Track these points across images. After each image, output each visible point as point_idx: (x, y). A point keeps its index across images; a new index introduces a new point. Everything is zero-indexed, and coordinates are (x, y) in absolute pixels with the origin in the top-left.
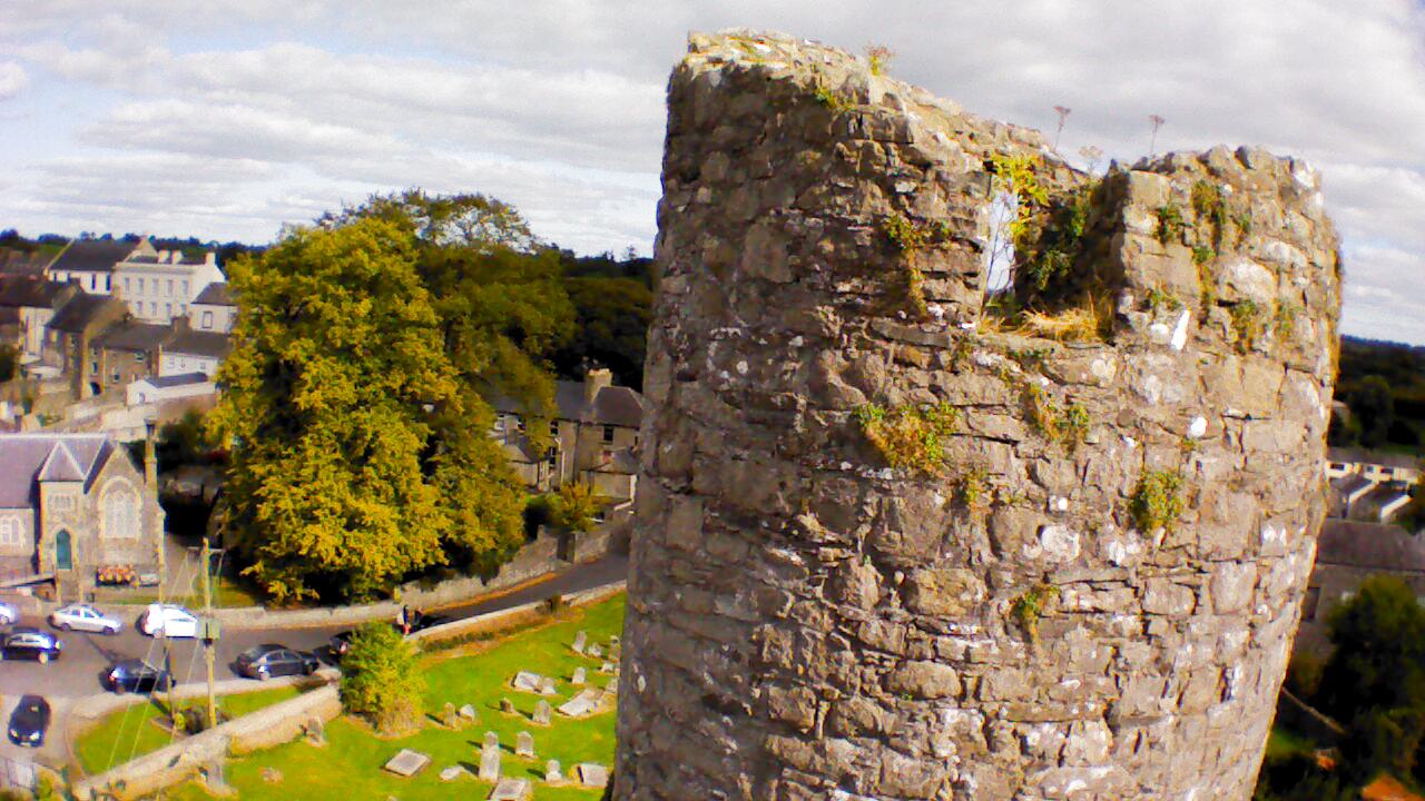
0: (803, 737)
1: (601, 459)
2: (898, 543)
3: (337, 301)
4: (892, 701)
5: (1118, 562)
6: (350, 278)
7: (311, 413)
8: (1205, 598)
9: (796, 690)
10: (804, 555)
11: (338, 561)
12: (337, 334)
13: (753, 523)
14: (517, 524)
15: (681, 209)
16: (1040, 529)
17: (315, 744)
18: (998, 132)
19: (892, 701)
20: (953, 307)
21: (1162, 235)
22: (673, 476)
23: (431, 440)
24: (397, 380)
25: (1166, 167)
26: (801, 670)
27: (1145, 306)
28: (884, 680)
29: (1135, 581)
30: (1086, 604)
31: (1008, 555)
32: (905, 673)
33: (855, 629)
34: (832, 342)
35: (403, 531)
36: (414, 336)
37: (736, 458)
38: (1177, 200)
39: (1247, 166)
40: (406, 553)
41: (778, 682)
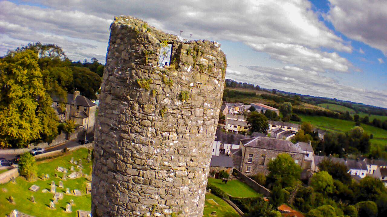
0: (127, 133)
1: (76, 114)
2: (142, 100)
3: (20, 70)
4: (141, 127)
5: (177, 105)
6: (23, 65)
7: (12, 99)
8: (193, 113)
9: (125, 125)
10: (127, 102)
11: (17, 137)
12: (19, 78)
13: (119, 98)
14: (56, 131)
15: (112, 48)
16: (164, 99)
17: (13, 183)
18: (168, 36)
19: (141, 127)
20: (152, 64)
21: (187, 54)
22: (107, 91)
23: (38, 107)
24: (32, 91)
25: (189, 43)
26: (126, 122)
27: (183, 65)
28: (139, 123)
29: (180, 109)
30: (172, 112)
31: (159, 103)
32: (142, 122)
33: (135, 114)
34: (134, 69)
35: (31, 130)
36: (36, 80)
37: (118, 87)
38: (190, 48)
39: (204, 43)
40: (32, 135)
41: (123, 124)
